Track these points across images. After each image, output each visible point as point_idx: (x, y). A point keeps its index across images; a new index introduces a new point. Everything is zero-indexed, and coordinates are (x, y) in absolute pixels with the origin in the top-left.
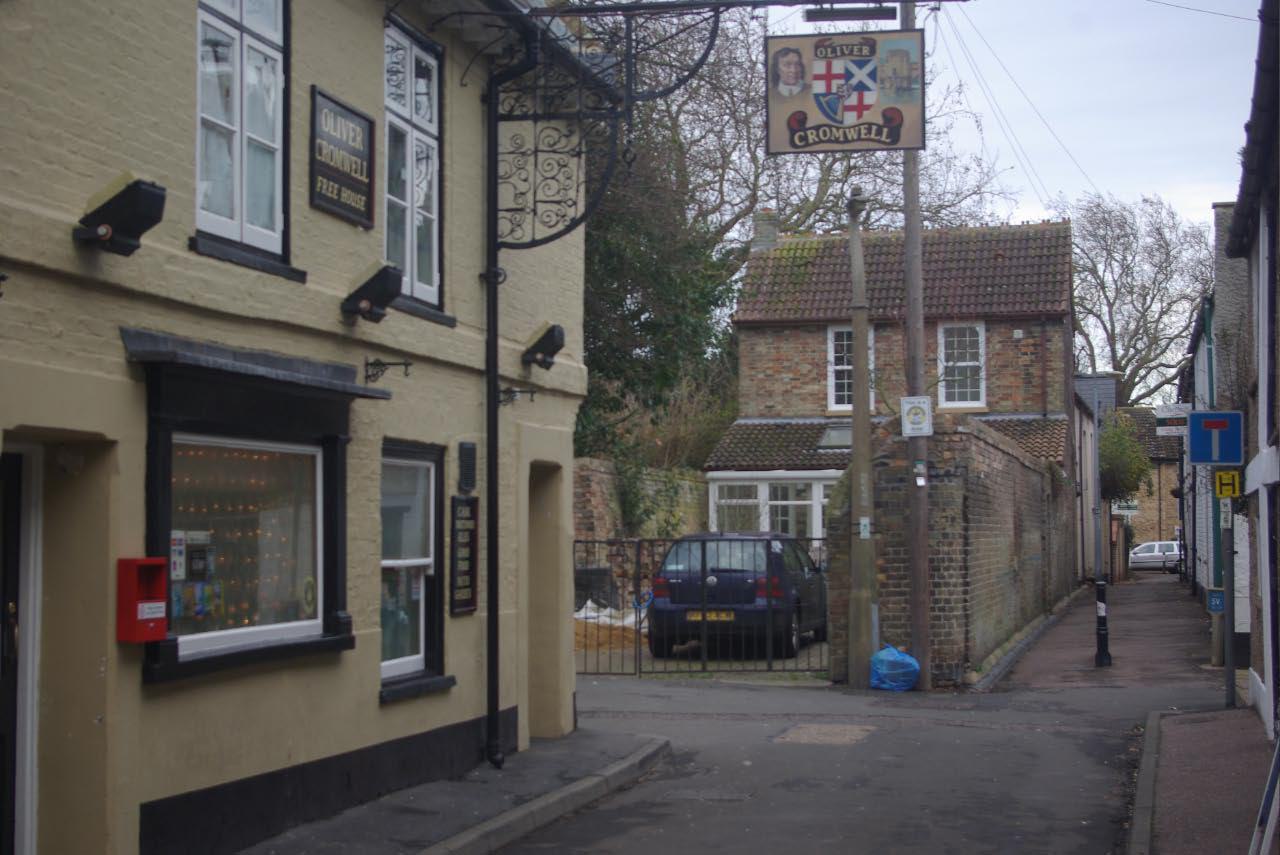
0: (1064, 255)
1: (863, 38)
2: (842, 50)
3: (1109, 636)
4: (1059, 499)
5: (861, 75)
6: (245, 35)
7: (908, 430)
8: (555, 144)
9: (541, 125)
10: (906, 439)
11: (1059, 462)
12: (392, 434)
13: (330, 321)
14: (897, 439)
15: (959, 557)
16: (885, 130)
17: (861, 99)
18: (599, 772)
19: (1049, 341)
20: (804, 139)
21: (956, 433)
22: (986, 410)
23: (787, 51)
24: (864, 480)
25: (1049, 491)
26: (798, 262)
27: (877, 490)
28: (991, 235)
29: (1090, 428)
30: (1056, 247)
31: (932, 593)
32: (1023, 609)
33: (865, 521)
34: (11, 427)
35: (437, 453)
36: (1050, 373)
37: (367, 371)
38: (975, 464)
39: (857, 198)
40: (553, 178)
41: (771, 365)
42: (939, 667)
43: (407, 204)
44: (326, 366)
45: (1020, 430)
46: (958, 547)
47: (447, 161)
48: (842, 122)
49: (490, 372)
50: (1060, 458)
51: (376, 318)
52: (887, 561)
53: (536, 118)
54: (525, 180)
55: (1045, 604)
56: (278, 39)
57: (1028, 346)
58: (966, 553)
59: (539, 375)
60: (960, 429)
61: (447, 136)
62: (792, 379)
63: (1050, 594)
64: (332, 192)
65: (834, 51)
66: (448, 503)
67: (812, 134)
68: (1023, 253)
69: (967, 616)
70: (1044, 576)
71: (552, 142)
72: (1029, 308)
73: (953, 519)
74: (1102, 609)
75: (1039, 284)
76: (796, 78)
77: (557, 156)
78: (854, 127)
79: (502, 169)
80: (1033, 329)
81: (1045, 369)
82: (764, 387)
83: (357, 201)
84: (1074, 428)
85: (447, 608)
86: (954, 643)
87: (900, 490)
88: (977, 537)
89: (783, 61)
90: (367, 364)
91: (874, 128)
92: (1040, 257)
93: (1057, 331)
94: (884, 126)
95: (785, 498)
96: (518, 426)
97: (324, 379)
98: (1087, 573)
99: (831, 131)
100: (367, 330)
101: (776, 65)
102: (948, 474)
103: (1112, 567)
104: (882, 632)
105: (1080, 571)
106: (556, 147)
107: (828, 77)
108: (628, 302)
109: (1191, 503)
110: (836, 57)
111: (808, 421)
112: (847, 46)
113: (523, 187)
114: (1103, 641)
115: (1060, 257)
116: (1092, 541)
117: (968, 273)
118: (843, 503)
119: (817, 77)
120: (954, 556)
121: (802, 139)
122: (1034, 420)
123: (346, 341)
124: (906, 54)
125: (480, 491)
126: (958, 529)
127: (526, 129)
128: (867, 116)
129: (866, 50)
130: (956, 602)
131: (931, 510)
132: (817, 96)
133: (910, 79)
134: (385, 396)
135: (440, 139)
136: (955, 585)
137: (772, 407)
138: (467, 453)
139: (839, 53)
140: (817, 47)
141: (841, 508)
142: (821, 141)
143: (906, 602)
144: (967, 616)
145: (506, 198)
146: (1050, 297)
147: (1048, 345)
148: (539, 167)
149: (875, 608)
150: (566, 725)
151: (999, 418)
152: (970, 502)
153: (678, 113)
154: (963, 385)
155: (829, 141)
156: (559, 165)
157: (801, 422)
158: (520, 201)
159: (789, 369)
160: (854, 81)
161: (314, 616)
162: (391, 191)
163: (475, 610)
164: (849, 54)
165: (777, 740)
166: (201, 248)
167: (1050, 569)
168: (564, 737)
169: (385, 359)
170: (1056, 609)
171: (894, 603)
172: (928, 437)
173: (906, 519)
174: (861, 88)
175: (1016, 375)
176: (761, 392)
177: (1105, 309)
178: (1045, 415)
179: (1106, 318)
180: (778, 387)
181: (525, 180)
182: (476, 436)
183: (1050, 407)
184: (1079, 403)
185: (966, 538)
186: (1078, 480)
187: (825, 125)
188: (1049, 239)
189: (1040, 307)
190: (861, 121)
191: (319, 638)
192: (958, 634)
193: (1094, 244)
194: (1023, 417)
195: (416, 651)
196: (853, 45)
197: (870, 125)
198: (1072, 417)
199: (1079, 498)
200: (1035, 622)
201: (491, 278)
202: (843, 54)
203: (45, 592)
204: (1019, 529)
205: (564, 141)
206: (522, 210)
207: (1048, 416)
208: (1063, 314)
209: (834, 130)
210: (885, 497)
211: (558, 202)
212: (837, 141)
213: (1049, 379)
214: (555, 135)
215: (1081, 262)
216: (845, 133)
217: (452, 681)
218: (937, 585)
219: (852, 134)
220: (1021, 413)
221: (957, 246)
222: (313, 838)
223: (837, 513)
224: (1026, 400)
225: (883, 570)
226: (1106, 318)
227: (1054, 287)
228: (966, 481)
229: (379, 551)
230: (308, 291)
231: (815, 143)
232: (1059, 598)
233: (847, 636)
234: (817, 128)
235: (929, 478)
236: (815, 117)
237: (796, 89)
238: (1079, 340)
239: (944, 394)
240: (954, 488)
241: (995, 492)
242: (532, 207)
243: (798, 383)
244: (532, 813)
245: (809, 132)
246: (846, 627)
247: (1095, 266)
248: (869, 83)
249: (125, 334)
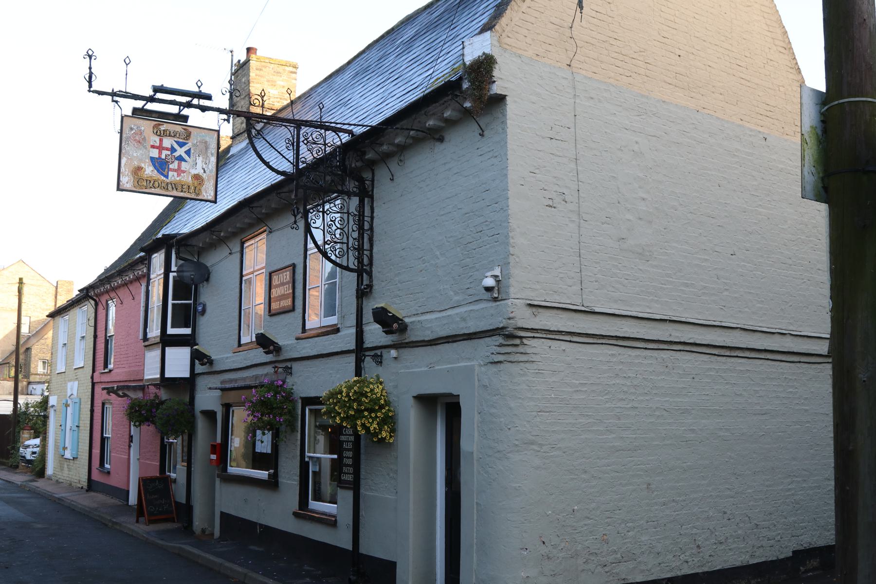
10: (42, 443)
17: (179, 166)
62: (512, 10)
109: (375, 103)
174: (180, 159)
222: (269, 407)
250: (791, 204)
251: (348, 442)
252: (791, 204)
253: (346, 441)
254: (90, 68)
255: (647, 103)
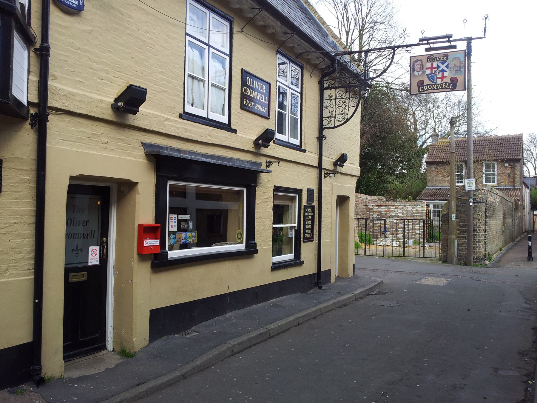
0: (521, 143)
1: (444, 54)
2: (436, 59)
3: (532, 252)
4: (518, 210)
5: (443, 67)
6: (290, 89)
7: (467, 189)
8: (342, 96)
9: (337, 90)
10: (467, 191)
11: (518, 200)
12: (277, 185)
13: (250, 147)
14: (464, 191)
15: (483, 227)
16: (451, 84)
17: (443, 74)
18: (352, 292)
19: (516, 166)
20: (423, 89)
21: (483, 190)
22: (497, 185)
23: (417, 61)
24: (454, 204)
25: (514, 208)
26: (444, 146)
27: (457, 206)
28: (499, 138)
29: (528, 191)
30: (518, 141)
31: (474, 237)
32: (505, 241)
33: (453, 215)
34: (75, 174)
35: (299, 192)
36: (516, 175)
37: (267, 164)
38: (489, 199)
39: (452, 120)
40: (341, 106)
41: (436, 173)
42: (476, 259)
43: (277, 109)
44: (248, 162)
45: (506, 191)
46: (483, 223)
47: (304, 100)
48: (436, 83)
49: (320, 167)
50: (518, 199)
51: (267, 147)
52: (460, 227)
53: (336, 88)
54: (333, 108)
55: (512, 239)
56: (228, 53)
57: (509, 168)
58: (486, 225)
59: (339, 169)
60: (484, 188)
61: (304, 93)
63: (514, 236)
64: (251, 105)
65: (434, 59)
66: (303, 207)
67: (426, 87)
68: (508, 143)
69: (485, 244)
70: (513, 231)
71: (341, 95)
72: (510, 157)
73: (482, 215)
74: (530, 244)
75: (513, 151)
76: (421, 69)
77: (342, 100)
78: (440, 84)
79: (325, 105)
80: (511, 163)
81: (514, 174)
82: (434, 179)
83: (264, 110)
84: (523, 190)
85: (302, 240)
86: (481, 252)
87: (465, 206)
88: (490, 220)
89: (416, 64)
90: (267, 162)
91: (447, 84)
92: (514, 144)
93: (518, 164)
94: (451, 83)
95: (438, 208)
96: (332, 184)
97: (247, 166)
98: (526, 230)
99: (432, 86)
100: (264, 151)
101: (414, 65)
102: (480, 202)
103: (534, 228)
104: (458, 248)
105: (524, 229)
106: (342, 97)
107: (431, 68)
108: (520, 203)
110: (434, 61)
111: (446, 188)
112: (438, 57)
113: (332, 110)
114: (530, 253)
115: (519, 144)
116: (528, 223)
117: (492, 148)
118: (447, 210)
119: (428, 68)
120: (482, 226)
121: (422, 89)
122: (511, 188)
123: (257, 154)
124: (459, 59)
125: (315, 203)
126: (483, 218)
127: (333, 92)
128: (445, 80)
129: (445, 58)
130: (482, 240)
131: (474, 213)
132: (427, 75)
133: (460, 67)
134: (269, 172)
135: (301, 94)
136: (482, 235)
137: (436, 184)
138: (310, 192)
139: (435, 60)
140: (428, 59)
141: (446, 211)
142: (429, 90)
143: (466, 239)
144: (485, 244)
145: (326, 113)
146: (516, 154)
147: (515, 167)
148: (337, 103)
149: (456, 241)
150: (351, 273)
151: (501, 187)
152: (487, 210)
153: (415, 111)
154: (490, 178)
155: (432, 89)
156: (343, 102)
157: (444, 188)
158: (331, 114)
159: (441, 174)
160: (440, 69)
161: (242, 243)
162: (291, 114)
163: (314, 240)
164: (439, 60)
165: (417, 282)
166: (183, 117)
167: (514, 229)
168: (349, 278)
169: (272, 160)
170: (516, 240)
171: (462, 240)
172: (474, 191)
173: (466, 215)
174: (443, 71)
175: (506, 176)
176: (433, 180)
177: (533, 160)
178: (514, 187)
179: (533, 163)
180: (437, 179)
181: (333, 108)
182: (314, 186)
183: (516, 185)
184: (525, 184)
185: (486, 221)
186: (524, 205)
187: (430, 84)
188: (516, 139)
189: (513, 157)
190: (443, 82)
191: (244, 250)
192: (483, 250)
193: (531, 143)
194: (507, 187)
195: (291, 253)
196: (440, 57)
197: (446, 83)
198: (522, 187)
199: (524, 210)
200: (509, 244)
201: (321, 139)
202: (437, 60)
203: (117, 235)
204: (504, 218)
205: (344, 94)
206: (331, 117)
207: (515, 187)
208: (520, 159)
209: (433, 85)
210: (460, 208)
211: (342, 114)
212: (434, 89)
213: (515, 177)
214: (342, 93)
215: (527, 148)
216: (437, 86)
217: (303, 262)
218: (476, 235)
219: (439, 87)
220: (507, 186)
221: (491, 141)
223: (445, 213)
224: (508, 183)
225: (459, 230)
226: (533, 163)
227: (518, 152)
228: (486, 204)
229: (272, 222)
230: (238, 136)
231: (427, 90)
232: (517, 237)
233: (447, 249)
234: (427, 85)
235: (474, 203)
236: (427, 82)
237: (420, 73)
238: (525, 169)
239: (485, 181)
240: (482, 207)
241: (496, 207)
242: (334, 116)
243: (443, 178)
244: (320, 309)
245: (424, 87)
246: (447, 246)
247: (531, 149)
248: (446, 69)
249: (144, 144)
250: (480, 95)
251: (309, 216)
252: (480, 95)
253: (308, 216)
254: (485, 25)
255: (116, 87)
